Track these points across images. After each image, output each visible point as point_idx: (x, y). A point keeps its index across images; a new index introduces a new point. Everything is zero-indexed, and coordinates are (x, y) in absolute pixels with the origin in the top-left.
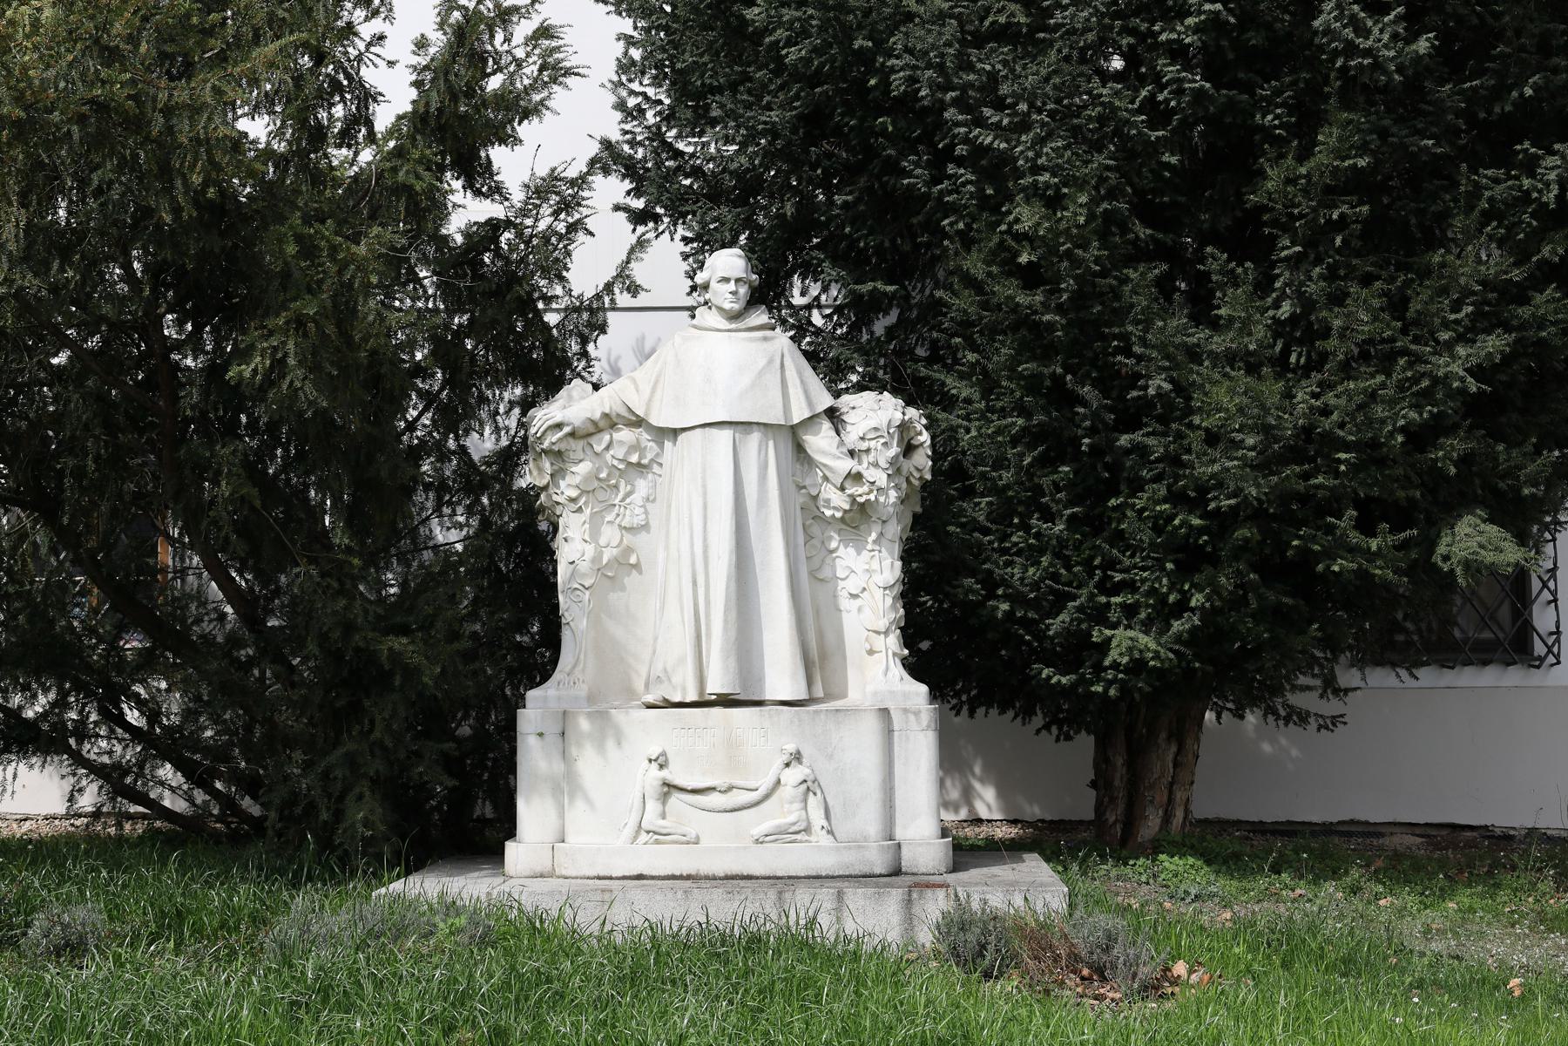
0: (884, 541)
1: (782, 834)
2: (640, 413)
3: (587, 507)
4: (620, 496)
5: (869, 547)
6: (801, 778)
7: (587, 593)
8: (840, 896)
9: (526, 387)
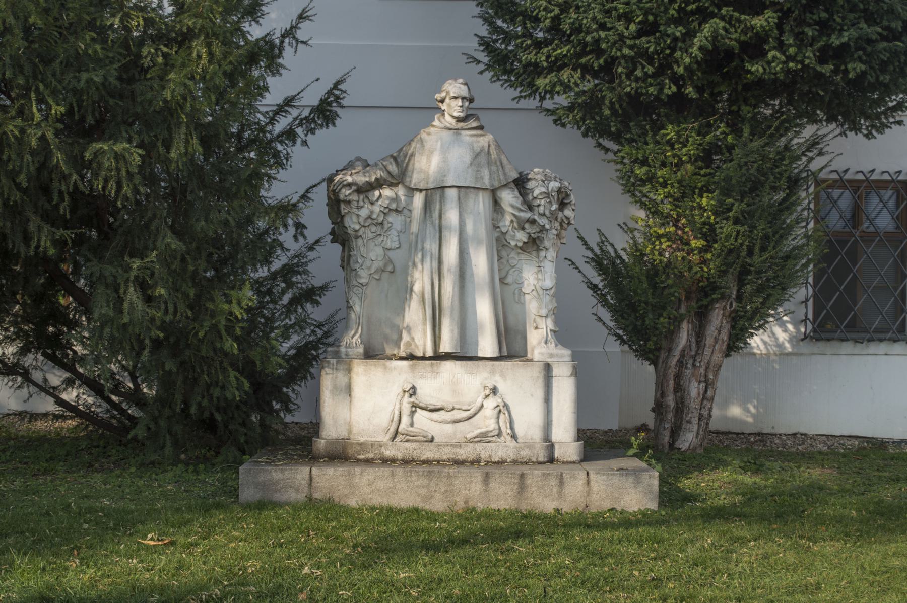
9: (246, 139)
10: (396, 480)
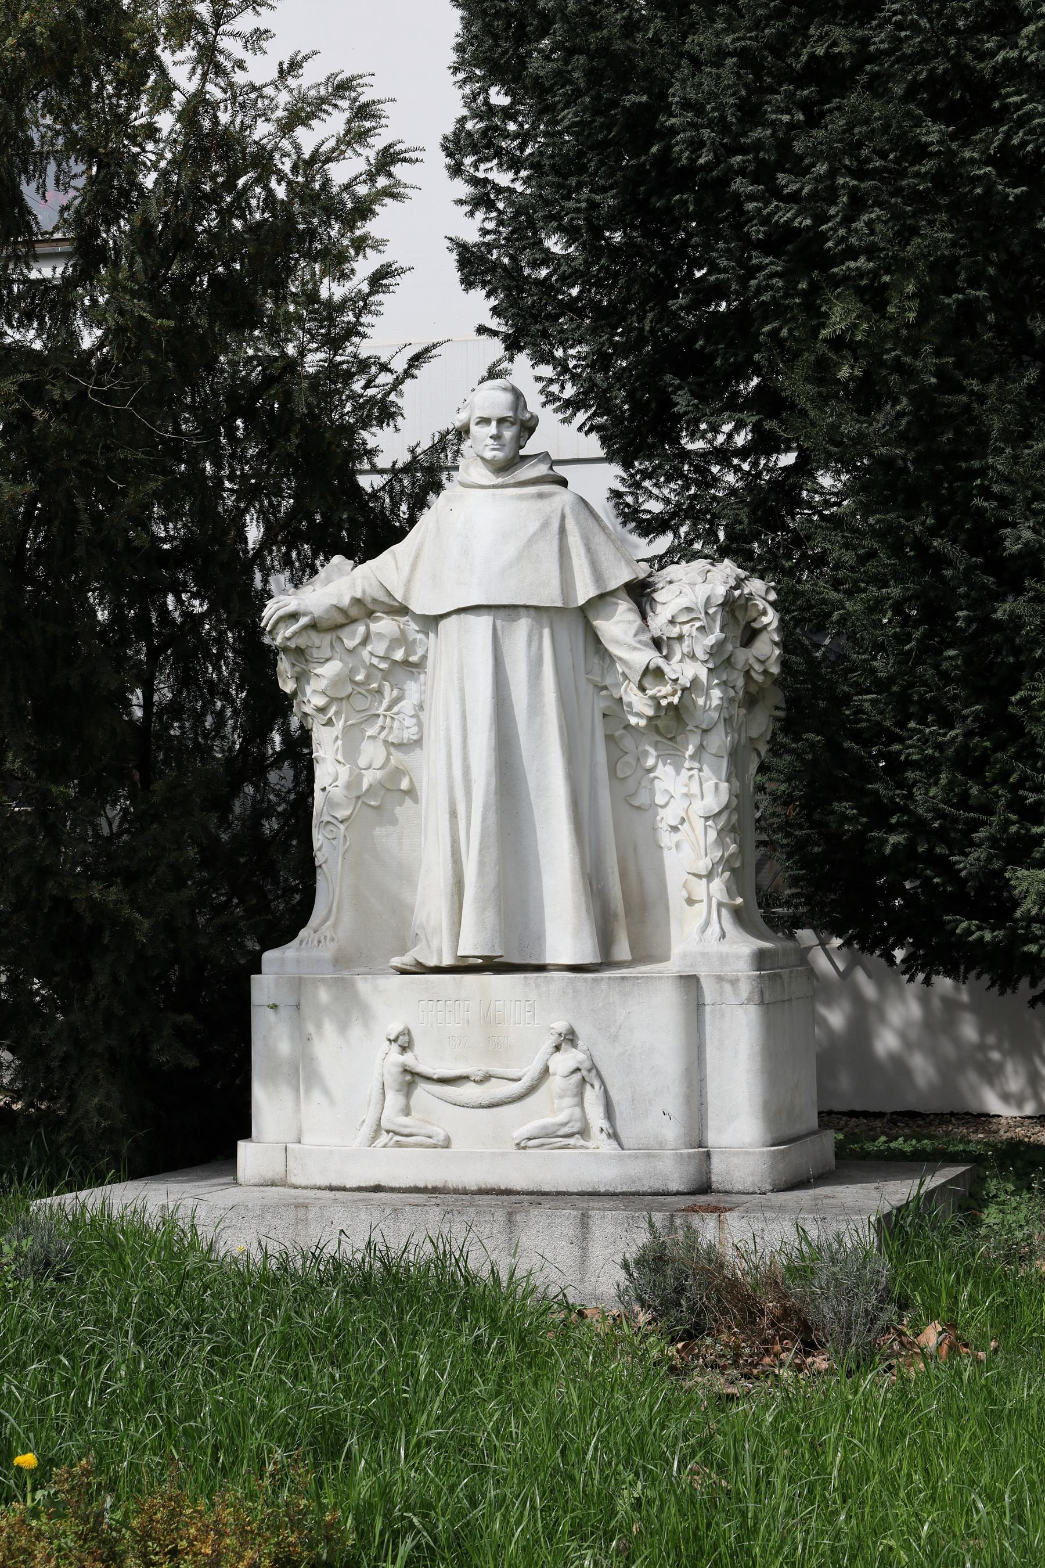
0: (706, 756)
1: (546, 1138)
2: (399, 597)
3: (339, 719)
4: (385, 704)
5: (687, 764)
6: (573, 1065)
7: (342, 827)
8: (584, 1222)
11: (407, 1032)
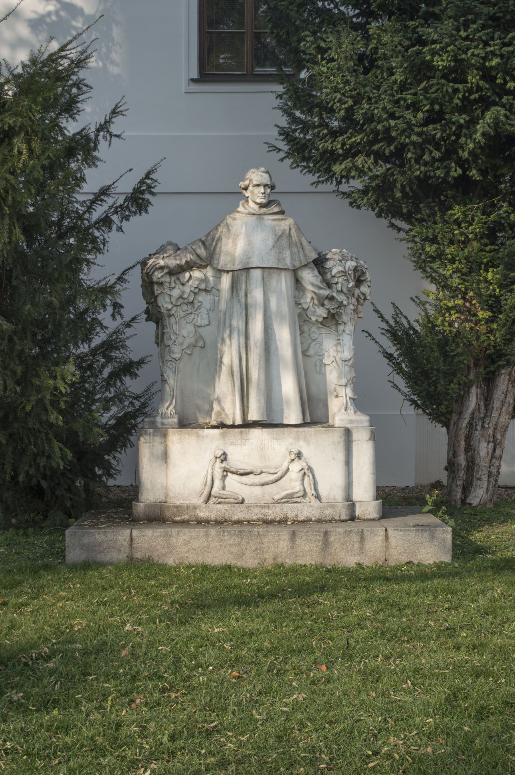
10: (210, 539)
11: (225, 454)
